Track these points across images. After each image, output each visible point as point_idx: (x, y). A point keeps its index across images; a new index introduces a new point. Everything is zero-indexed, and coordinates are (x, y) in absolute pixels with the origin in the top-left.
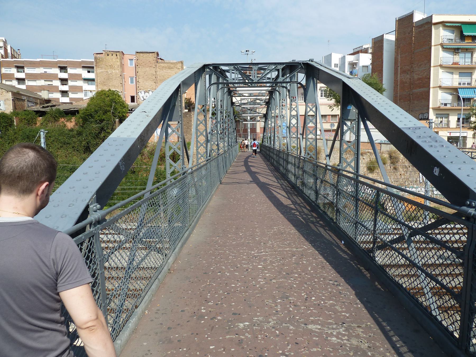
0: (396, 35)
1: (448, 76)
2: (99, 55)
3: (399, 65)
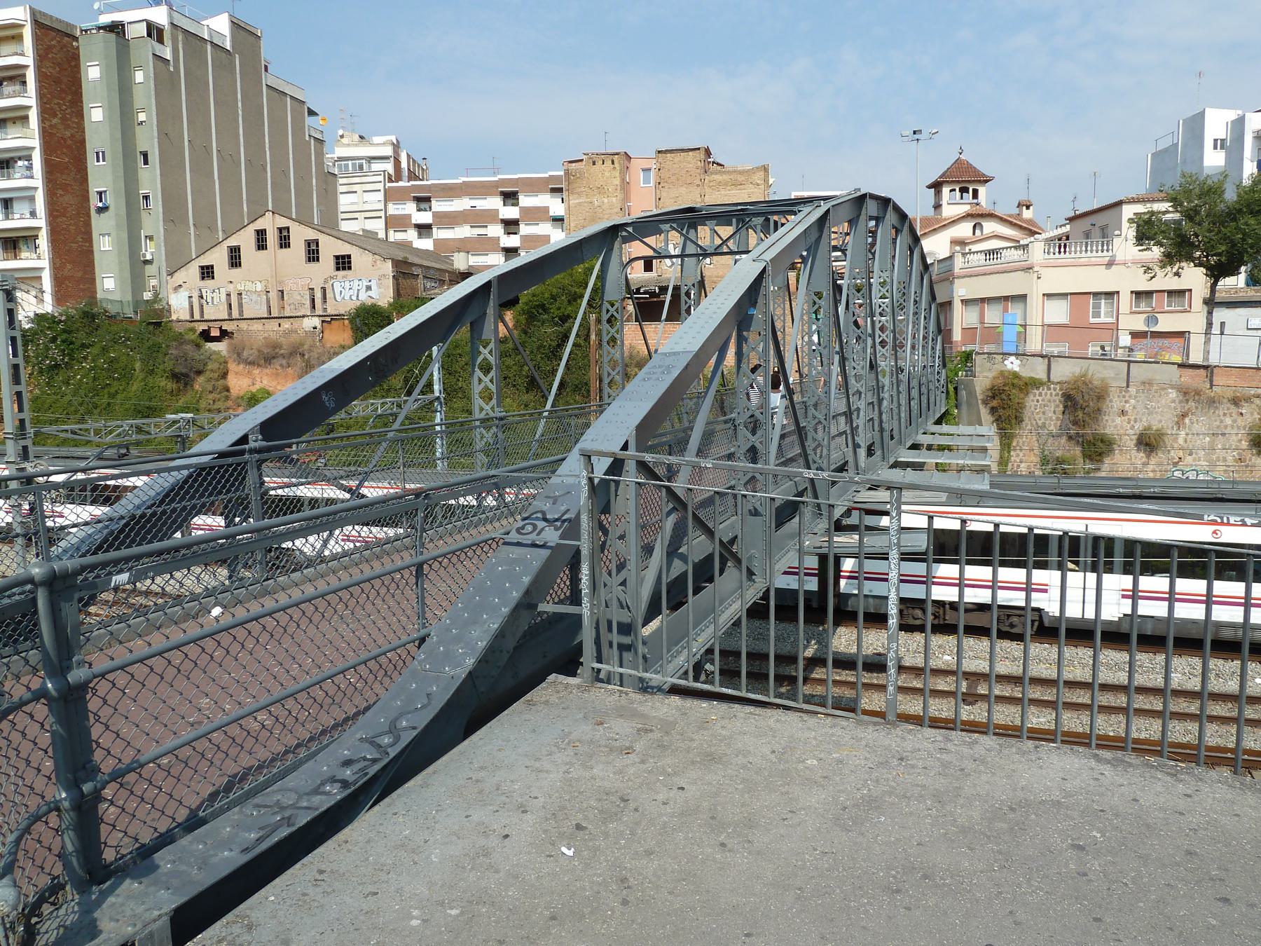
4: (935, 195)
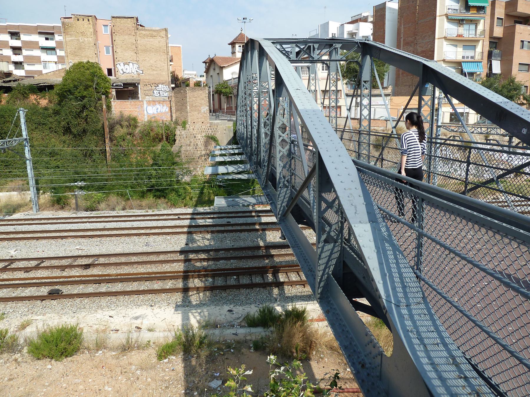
0: (399, 3)
1: (453, 48)
2: (67, 19)
3: (402, 36)
4: (232, 48)
